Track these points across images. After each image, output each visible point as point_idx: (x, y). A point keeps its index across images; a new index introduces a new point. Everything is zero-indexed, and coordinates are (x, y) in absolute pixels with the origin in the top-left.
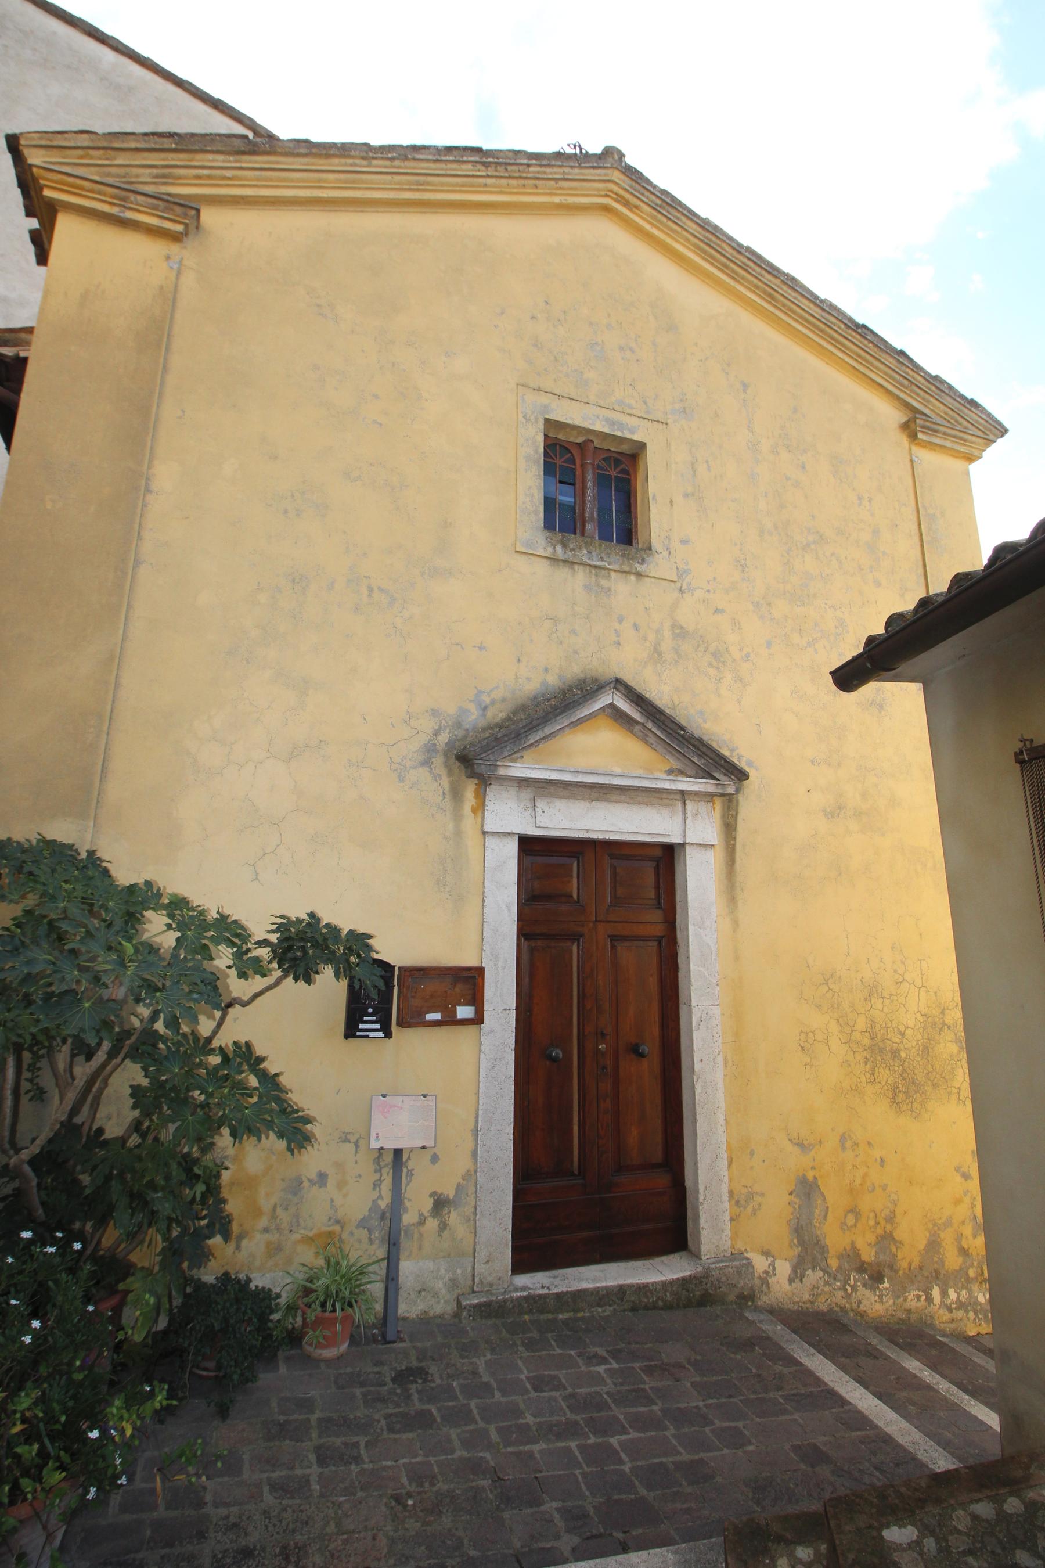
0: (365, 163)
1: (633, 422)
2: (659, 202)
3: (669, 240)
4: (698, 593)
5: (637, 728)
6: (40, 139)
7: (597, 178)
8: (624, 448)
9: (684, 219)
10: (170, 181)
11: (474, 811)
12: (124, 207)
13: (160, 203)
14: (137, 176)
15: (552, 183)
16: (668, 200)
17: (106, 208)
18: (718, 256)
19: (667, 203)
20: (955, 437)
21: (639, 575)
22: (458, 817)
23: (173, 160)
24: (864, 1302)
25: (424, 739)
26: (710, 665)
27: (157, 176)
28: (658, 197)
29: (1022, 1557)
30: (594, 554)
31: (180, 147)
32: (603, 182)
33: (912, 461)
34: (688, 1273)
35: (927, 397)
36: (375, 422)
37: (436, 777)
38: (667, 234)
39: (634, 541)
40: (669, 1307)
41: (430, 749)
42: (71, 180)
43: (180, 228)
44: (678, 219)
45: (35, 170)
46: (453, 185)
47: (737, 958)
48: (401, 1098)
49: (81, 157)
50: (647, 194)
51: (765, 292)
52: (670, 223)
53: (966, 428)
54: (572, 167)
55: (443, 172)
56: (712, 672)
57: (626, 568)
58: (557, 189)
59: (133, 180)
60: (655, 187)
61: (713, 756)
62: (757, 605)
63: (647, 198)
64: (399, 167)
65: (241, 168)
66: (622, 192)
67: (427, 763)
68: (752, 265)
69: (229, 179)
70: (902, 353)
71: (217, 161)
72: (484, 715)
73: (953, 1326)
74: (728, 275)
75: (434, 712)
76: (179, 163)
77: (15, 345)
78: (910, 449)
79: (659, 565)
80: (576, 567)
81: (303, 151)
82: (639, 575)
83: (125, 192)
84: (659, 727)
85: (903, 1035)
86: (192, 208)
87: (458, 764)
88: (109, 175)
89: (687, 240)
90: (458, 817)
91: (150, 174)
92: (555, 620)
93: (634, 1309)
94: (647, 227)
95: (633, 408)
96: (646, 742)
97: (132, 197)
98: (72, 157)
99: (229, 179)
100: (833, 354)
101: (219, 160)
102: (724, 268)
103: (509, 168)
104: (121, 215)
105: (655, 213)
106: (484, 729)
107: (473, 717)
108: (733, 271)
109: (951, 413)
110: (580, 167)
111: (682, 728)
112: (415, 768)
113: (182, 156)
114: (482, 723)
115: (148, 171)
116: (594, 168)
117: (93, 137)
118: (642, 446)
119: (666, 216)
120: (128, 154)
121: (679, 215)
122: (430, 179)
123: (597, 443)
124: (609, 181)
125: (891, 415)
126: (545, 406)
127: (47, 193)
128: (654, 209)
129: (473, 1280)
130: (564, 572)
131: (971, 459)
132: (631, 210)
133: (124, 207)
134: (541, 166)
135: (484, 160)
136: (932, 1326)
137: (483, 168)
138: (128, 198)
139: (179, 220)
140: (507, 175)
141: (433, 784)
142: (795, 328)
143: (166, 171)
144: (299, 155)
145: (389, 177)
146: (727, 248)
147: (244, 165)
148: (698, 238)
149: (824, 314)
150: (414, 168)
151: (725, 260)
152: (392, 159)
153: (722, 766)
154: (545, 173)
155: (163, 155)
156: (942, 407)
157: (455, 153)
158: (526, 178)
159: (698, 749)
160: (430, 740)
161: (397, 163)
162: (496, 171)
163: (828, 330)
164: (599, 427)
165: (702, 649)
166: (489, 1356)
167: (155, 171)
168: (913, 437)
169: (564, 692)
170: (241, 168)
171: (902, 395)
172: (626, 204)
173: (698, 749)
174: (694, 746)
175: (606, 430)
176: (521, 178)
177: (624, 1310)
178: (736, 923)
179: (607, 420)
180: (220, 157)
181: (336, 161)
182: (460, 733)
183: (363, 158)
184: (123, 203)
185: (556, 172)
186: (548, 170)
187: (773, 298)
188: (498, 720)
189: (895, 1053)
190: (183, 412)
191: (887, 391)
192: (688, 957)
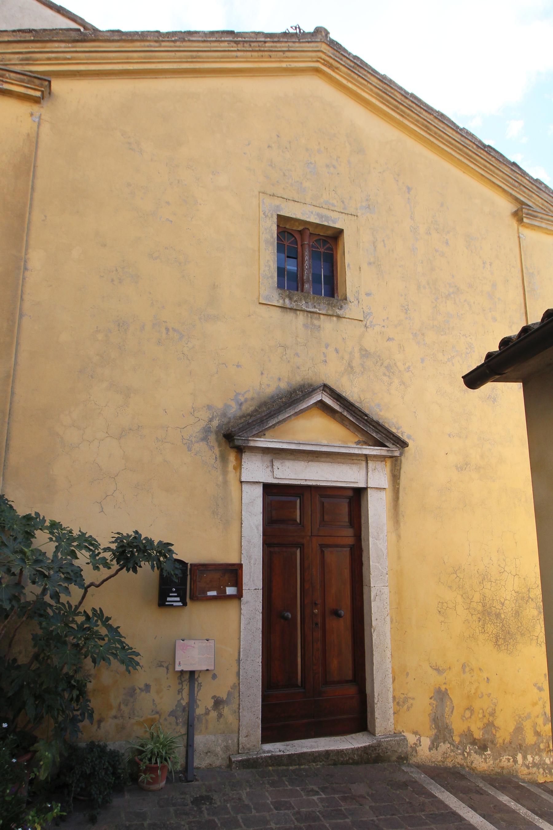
0: (157, 44)
1: (334, 215)
2: (352, 64)
3: (359, 91)
5: (337, 416)
8: (329, 233)
9: (369, 75)
13: (25, 77)
14: (10, 60)
15: (281, 54)
16: (358, 63)
19: (358, 65)
21: (338, 317)
22: (225, 472)
23: (32, 48)
24: (475, 762)
25: (203, 424)
27: (22, 60)
28: (351, 61)
30: (310, 303)
31: (36, 39)
32: (313, 52)
33: (519, 237)
35: (530, 193)
37: (211, 448)
39: (336, 295)
43: (38, 94)
46: (216, 58)
47: (399, 558)
50: (344, 59)
51: (423, 125)
52: (360, 79)
54: (294, 42)
57: (330, 312)
58: (284, 58)
62: (415, 335)
66: (327, 59)
68: (414, 106)
69: (69, 59)
71: (61, 47)
72: (240, 409)
75: (209, 407)
78: (518, 229)
79: (352, 310)
80: (298, 312)
81: (116, 38)
82: (338, 317)
89: (371, 90)
91: (18, 58)
94: (345, 82)
95: (335, 206)
99: (69, 59)
100: (468, 166)
101: (62, 47)
102: (395, 109)
103: (253, 44)
105: (349, 72)
107: (234, 410)
108: (402, 111)
109: (546, 204)
110: (299, 42)
111: (366, 415)
114: (239, 414)
115: (17, 56)
116: (309, 42)
121: (365, 73)
125: (506, 207)
128: (349, 69)
130: (290, 316)
132: (333, 71)
134: (273, 42)
135: (236, 39)
137: (235, 45)
140: (251, 49)
141: (209, 452)
143: (428, 125)
144: (113, 41)
145: (173, 54)
147: (78, 49)
149: (462, 139)
151: (396, 104)
152: (174, 41)
153: (391, 439)
154: (276, 47)
156: (540, 200)
159: (376, 428)
161: (178, 44)
162: (244, 47)
163: (465, 149)
164: (313, 219)
165: (379, 364)
167: (21, 56)
168: (520, 221)
171: (514, 193)
172: (331, 66)
173: (376, 428)
174: (373, 426)
175: (317, 221)
176: (260, 51)
178: (399, 537)
179: (318, 214)
180: (63, 45)
182: (225, 420)
183: (156, 41)
185: (283, 46)
186: (278, 45)
190: (46, 216)
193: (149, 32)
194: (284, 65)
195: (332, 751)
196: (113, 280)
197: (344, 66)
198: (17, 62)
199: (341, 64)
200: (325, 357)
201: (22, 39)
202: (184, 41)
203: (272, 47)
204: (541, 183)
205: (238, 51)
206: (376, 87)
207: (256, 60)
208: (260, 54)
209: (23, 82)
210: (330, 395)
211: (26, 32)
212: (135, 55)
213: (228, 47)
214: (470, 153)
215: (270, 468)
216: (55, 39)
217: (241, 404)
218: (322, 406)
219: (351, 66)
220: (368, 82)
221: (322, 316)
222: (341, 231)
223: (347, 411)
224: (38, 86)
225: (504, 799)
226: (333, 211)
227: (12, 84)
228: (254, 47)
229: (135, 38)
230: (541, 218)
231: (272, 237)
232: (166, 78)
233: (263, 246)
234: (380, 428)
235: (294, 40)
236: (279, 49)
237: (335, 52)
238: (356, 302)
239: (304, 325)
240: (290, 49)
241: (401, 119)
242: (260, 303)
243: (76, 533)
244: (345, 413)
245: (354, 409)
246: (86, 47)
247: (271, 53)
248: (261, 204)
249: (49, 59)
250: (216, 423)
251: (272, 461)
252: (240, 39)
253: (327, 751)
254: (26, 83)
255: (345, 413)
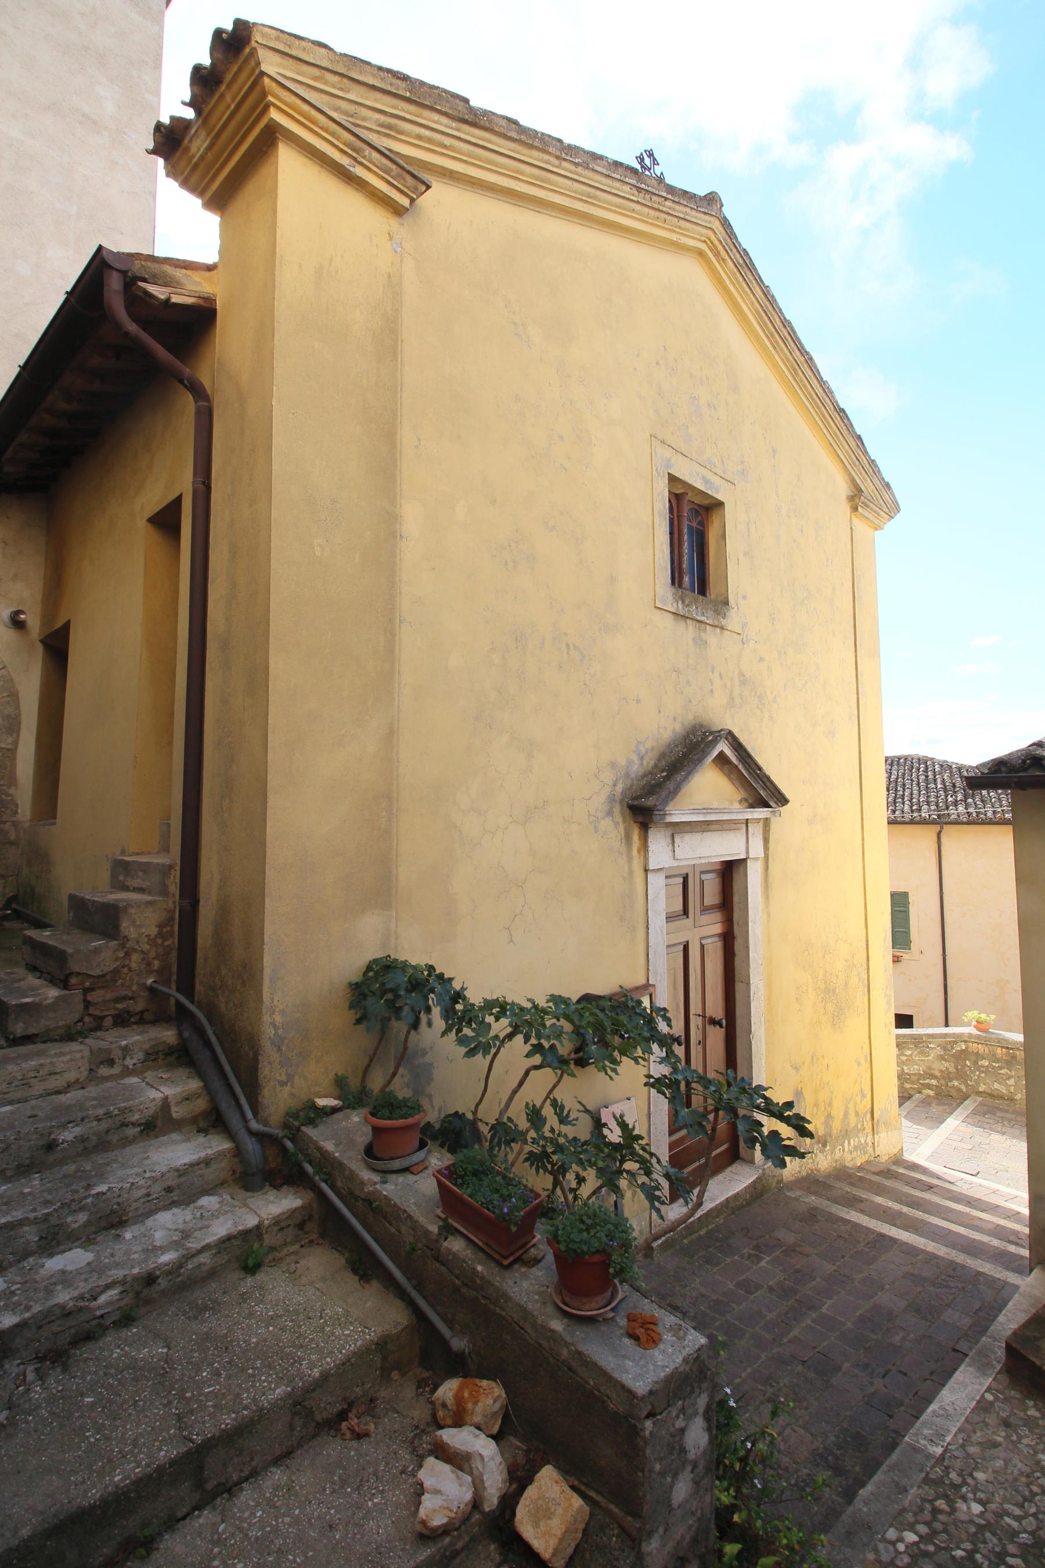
0: (556, 162)
1: (716, 480)
2: (741, 262)
3: (739, 300)
4: (752, 643)
6: (277, 39)
10: (393, 134)
12: (355, 160)
13: (394, 167)
14: (364, 119)
15: (676, 220)
18: (770, 325)
21: (722, 628)
22: (630, 858)
23: (403, 110)
25: (607, 790)
27: (382, 125)
29: (2, 1303)
37: (616, 824)
45: (266, 80)
49: (316, 79)
50: (734, 250)
51: (792, 366)
55: (608, 189)
57: (716, 623)
58: (676, 227)
60: (740, 245)
61: (772, 789)
64: (580, 175)
66: (717, 243)
68: (789, 339)
69: (445, 147)
70: (859, 438)
71: (441, 124)
72: (642, 764)
76: (408, 116)
77: (166, 285)
79: (733, 620)
80: (688, 621)
82: (722, 628)
88: (337, 109)
90: (630, 858)
94: (728, 282)
98: (306, 76)
99: (445, 147)
101: (442, 123)
103: (654, 198)
104: (351, 169)
105: (735, 270)
108: (776, 341)
110: (697, 211)
111: (760, 769)
112: (603, 818)
115: (377, 116)
116: (705, 213)
120: (362, 90)
122: (599, 193)
125: (843, 488)
130: (682, 624)
132: (719, 262)
133: (355, 160)
135: (639, 185)
137: (636, 193)
139: (401, 188)
141: (614, 828)
143: (393, 121)
146: (777, 319)
147: (463, 136)
149: (824, 395)
154: (674, 210)
158: (661, 211)
161: (579, 170)
164: (699, 485)
166: (698, 1280)
167: (382, 118)
168: (855, 509)
169: (686, 737)
171: (853, 473)
172: (717, 254)
175: (703, 488)
176: (658, 210)
178: (769, 915)
179: (704, 478)
180: (445, 120)
181: (536, 153)
182: (629, 782)
183: (557, 157)
184: (355, 155)
186: (677, 207)
187: (796, 373)
193: (550, 136)
194: (674, 237)
198: (374, 127)
205: (638, 202)
209: (388, 174)
211: (398, 78)
217: (642, 758)
218: (722, 760)
222: (720, 504)
224: (408, 188)
227: (369, 169)
234: (768, 784)
239: (694, 639)
241: (773, 352)
243: (542, 1003)
244: (741, 767)
249: (419, 137)
253: (727, 1199)
255: (741, 767)
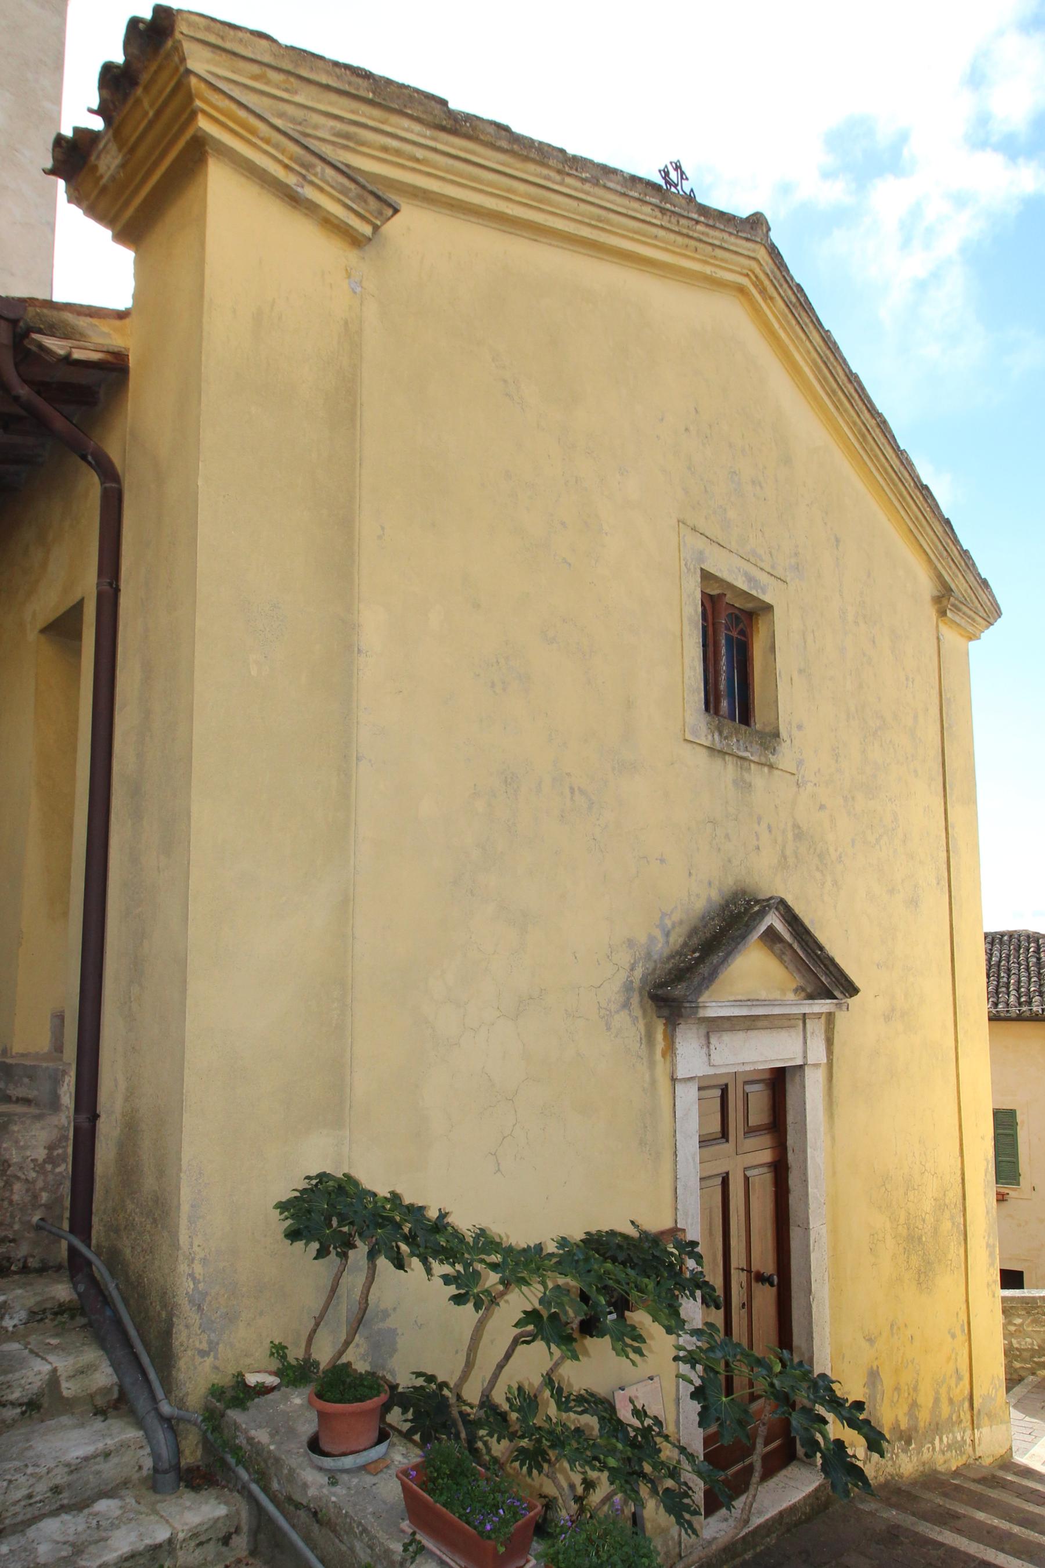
0: (558, 178)
1: (764, 578)
2: (794, 300)
3: (792, 348)
5: (778, 946)
7: (746, 253)
8: (749, 606)
9: (810, 325)
10: (351, 144)
11: (664, 1055)
12: (304, 177)
14: (316, 127)
15: (710, 248)
16: (802, 300)
17: (280, 173)
18: (831, 379)
19: (801, 304)
20: (969, 617)
21: (771, 767)
22: (652, 1065)
23: (364, 115)
24: (903, 1465)
25: (623, 976)
26: (818, 869)
27: (338, 135)
28: (794, 293)
30: (741, 742)
31: (378, 100)
33: (938, 638)
34: (817, 1484)
35: (957, 571)
36: (565, 561)
38: (792, 340)
39: (752, 724)
40: (809, 1519)
41: (628, 987)
42: (242, 114)
43: (367, 230)
44: (806, 325)
46: (629, 230)
47: (834, 1173)
48: (635, 1387)
49: (255, 78)
50: (785, 286)
51: (860, 431)
52: (797, 328)
53: (976, 608)
54: (731, 234)
56: (818, 875)
57: (763, 760)
59: (309, 131)
61: (837, 975)
62: (845, 798)
63: (785, 292)
65: (435, 150)
66: (762, 277)
67: (626, 1005)
68: (857, 397)
69: (417, 160)
71: (412, 132)
72: (667, 942)
73: (946, 1466)
74: (833, 402)
75: (630, 943)
76: (371, 123)
77: (66, 337)
78: (937, 626)
79: (785, 757)
80: (727, 757)
82: (771, 767)
83: (310, 156)
84: (802, 947)
85: (924, 1221)
86: (390, 205)
87: (650, 1002)
88: (281, 115)
89: (808, 352)
90: (652, 1065)
91: (332, 128)
92: (713, 822)
93: (788, 1530)
94: (776, 326)
95: (762, 560)
96: (782, 961)
97: (320, 166)
100: (898, 512)
101: (413, 130)
103: (683, 221)
104: (299, 190)
105: (786, 311)
106: (671, 957)
107: (661, 948)
108: (839, 400)
109: (969, 590)
110: (737, 236)
111: (821, 948)
112: (617, 1012)
113: (376, 113)
114: (666, 952)
116: (747, 239)
117: (274, 47)
118: (769, 608)
119: (796, 319)
120: (313, 90)
121: (807, 320)
123: (729, 598)
124: (754, 259)
125: (925, 585)
126: (701, 553)
127: (203, 123)
128: (787, 306)
129: (680, 1546)
130: (719, 762)
131: (973, 637)
133: (304, 177)
134: (707, 225)
135: (663, 205)
136: (935, 1471)
137: (659, 215)
138: (313, 166)
140: (677, 229)
141: (631, 1025)
142: (875, 477)
143: (353, 129)
145: (574, 204)
147: (440, 146)
148: (819, 354)
149: (902, 469)
150: (602, 199)
151: (835, 386)
153: (842, 985)
154: (707, 235)
155: (355, 105)
156: (965, 585)
157: (639, 186)
158: (691, 238)
159: (827, 969)
160: (628, 977)
161: (587, 187)
162: (670, 222)
163: (900, 484)
164: (741, 584)
165: (812, 850)
167: (339, 126)
168: (942, 613)
170: (435, 150)
172: (763, 291)
173: (827, 969)
174: (825, 965)
177: (783, 1534)
178: (833, 1138)
181: (532, 167)
182: (650, 965)
183: (559, 172)
184: (303, 172)
185: (715, 236)
186: (711, 232)
188: (678, 947)
189: (920, 1238)
190: (383, 528)
191: (929, 558)
192: (806, 1181)
194: (708, 270)
195: (785, 1510)
196: (493, 685)
197: (782, 297)
199: (779, 294)
200: (758, 839)
201: (353, 91)
202: (597, 184)
203: (703, 234)
204: (970, 558)
205: (662, 227)
206: (816, 351)
207: (678, 250)
208: (687, 241)
209: (346, 195)
210: (782, 916)
212: (522, 187)
213: (650, 216)
214: (905, 493)
215: (705, 1049)
216: (409, 112)
218: (771, 936)
219: (791, 302)
220: (808, 337)
221: (752, 765)
223: (799, 942)
224: (371, 213)
225: (981, 1516)
226: (762, 569)
227: (321, 190)
228: (683, 226)
229: (533, 154)
230: (964, 614)
231: (696, 611)
232: (550, 245)
233: (687, 629)
234: (832, 968)
235: (731, 230)
236: (710, 241)
237: (776, 269)
238: (789, 742)
240: (724, 245)
242: (685, 740)
244: (796, 946)
245: (808, 938)
246: (453, 146)
247: (697, 244)
248: (682, 544)
249: (385, 149)
250: (638, 973)
251: (708, 1036)
252: (668, 206)
254: (350, 199)
255: (796, 946)
